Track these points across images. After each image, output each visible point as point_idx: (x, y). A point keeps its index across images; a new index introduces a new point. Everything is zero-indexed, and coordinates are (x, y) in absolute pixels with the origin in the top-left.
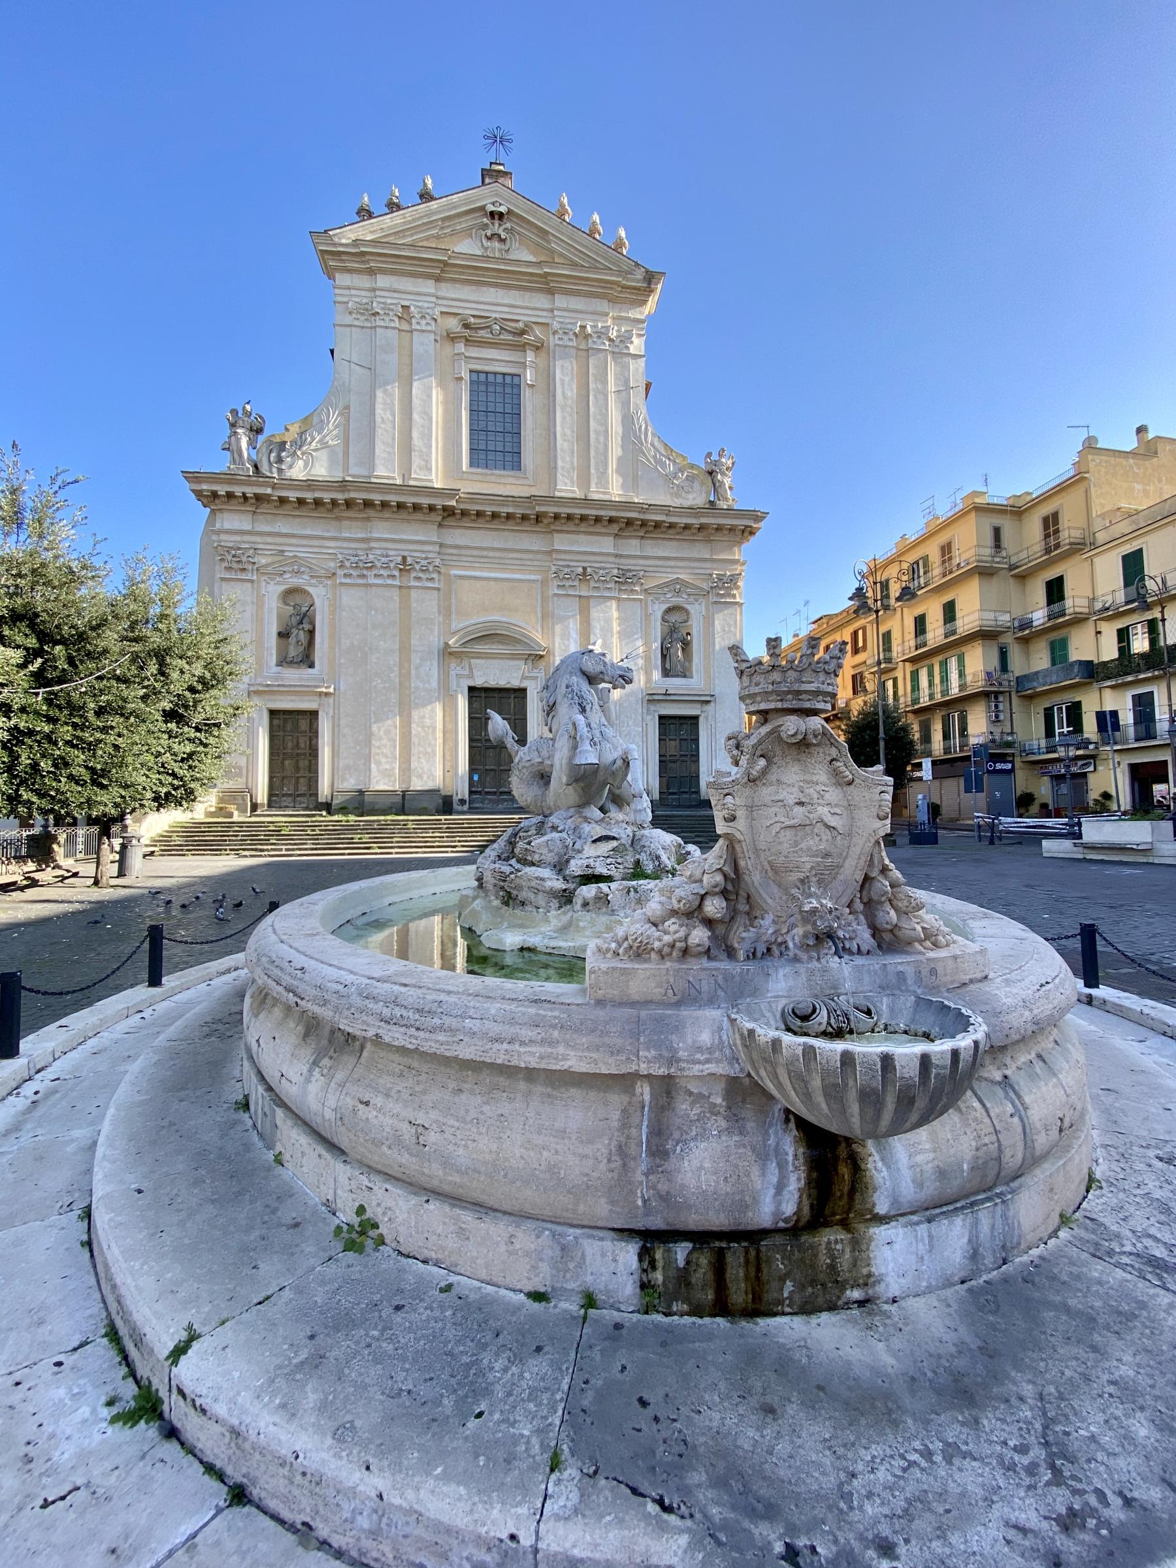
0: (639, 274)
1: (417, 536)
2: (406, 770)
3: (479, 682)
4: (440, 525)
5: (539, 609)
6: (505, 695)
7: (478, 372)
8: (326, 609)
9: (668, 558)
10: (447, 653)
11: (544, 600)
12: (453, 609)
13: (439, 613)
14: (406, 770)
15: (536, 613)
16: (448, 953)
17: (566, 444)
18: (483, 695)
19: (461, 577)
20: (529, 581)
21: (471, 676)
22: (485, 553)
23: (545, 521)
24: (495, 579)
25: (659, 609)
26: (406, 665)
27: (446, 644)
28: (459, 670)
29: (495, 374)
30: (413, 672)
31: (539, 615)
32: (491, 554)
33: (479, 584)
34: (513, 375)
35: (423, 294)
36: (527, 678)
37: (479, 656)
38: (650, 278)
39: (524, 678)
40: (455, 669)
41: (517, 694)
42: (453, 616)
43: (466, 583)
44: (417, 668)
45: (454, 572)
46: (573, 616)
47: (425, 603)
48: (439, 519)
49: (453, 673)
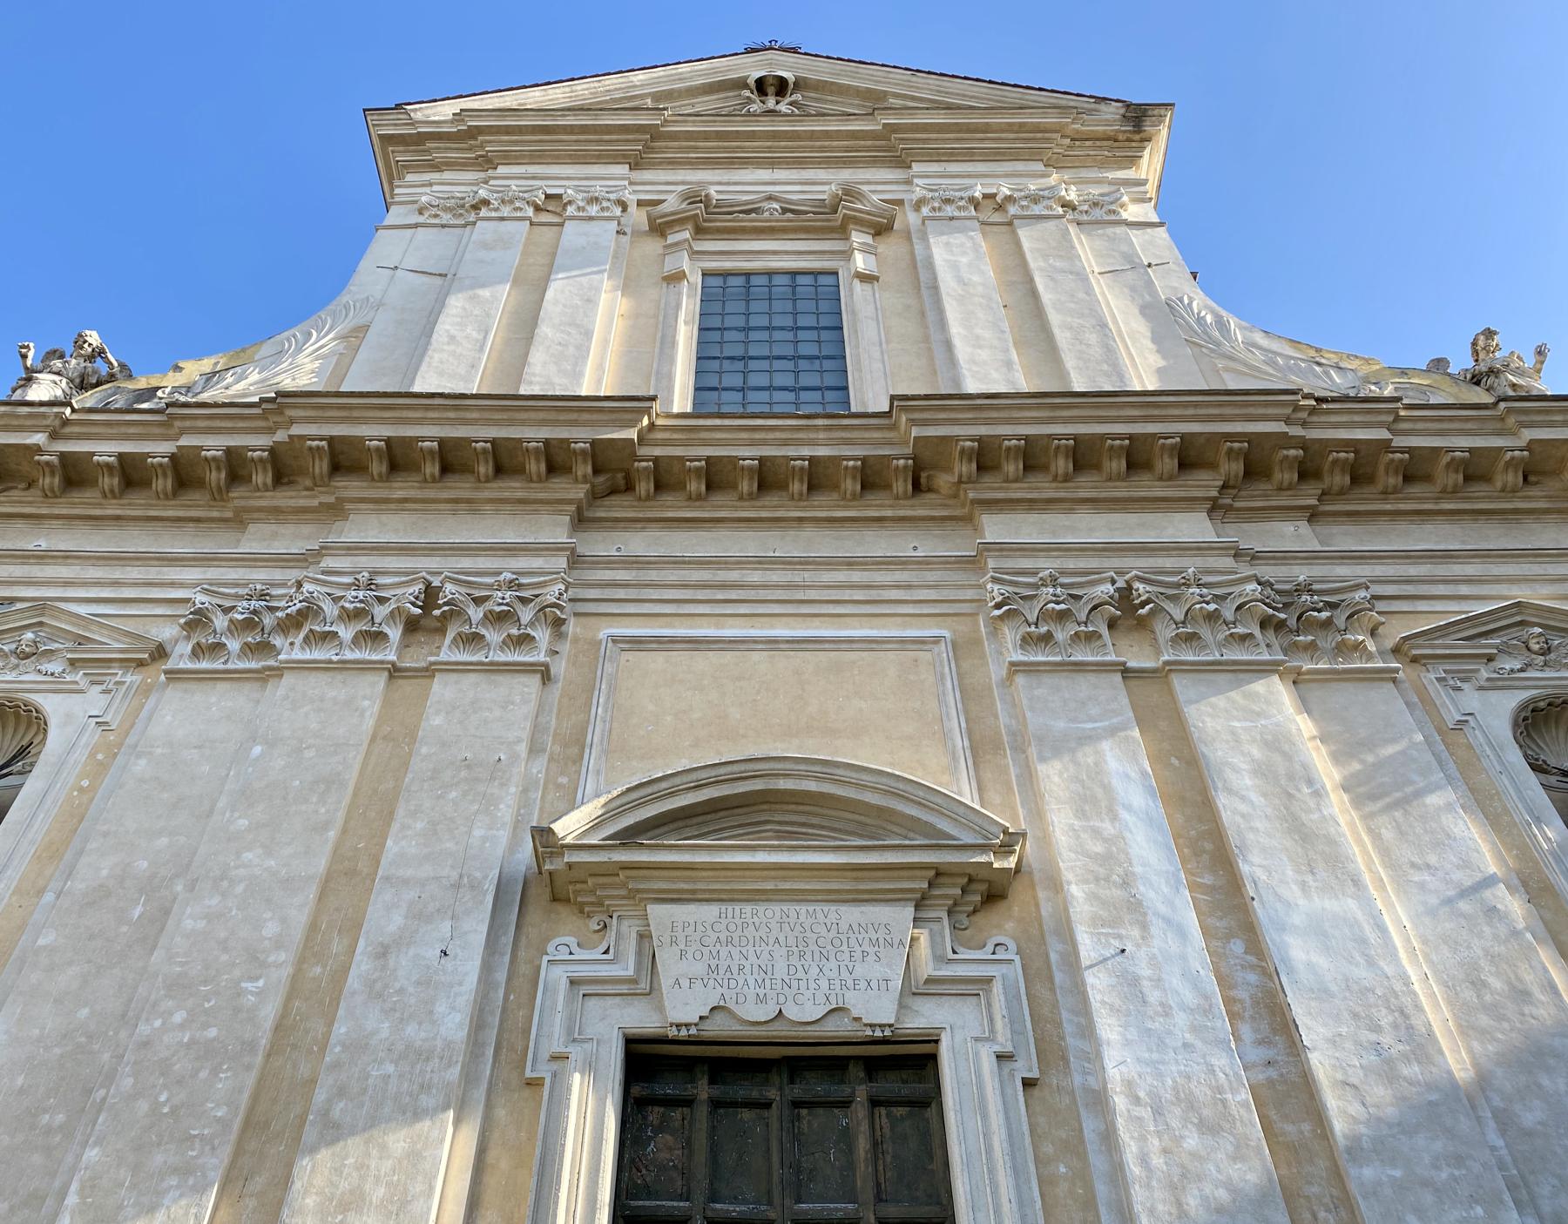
0: (1112, 112)
1: (504, 542)
2: (395, 738)
3: (683, 1006)
4: (581, 521)
5: (955, 724)
6: (818, 1087)
7: (726, 274)
8: (80, 755)
9: (1447, 556)
10: (552, 887)
11: (971, 696)
12: (595, 735)
13: (534, 750)
14: (395, 738)
15: (945, 736)
16: (1237, 947)
17: (984, 355)
18: (703, 1090)
19: (637, 643)
20: (903, 642)
21: (645, 984)
22: (734, 576)
23: (944, 481)
24: (773, 643)
25: (1496, 713)
26: (337, 946)
27: (543, 835)
28: (591, 962)
29: (770, 274)
30: (362, 965)
31: (960, 742)
32: (755, 577)
33: (704, 662)
34: (815, 274)
35: (613, 178)
36: (934, 988)
37: (689, 888)
38: (1138, 117)
39: (915, 990)
40: (567, 952)
41: (890, 1085)
42: (592, 759)
43: (656, 661)
44: (383, 953)
45: (606, 631)
46: (1112, 732)
47: (478, 713)
48: (580, 492)
49: (556, 977)
